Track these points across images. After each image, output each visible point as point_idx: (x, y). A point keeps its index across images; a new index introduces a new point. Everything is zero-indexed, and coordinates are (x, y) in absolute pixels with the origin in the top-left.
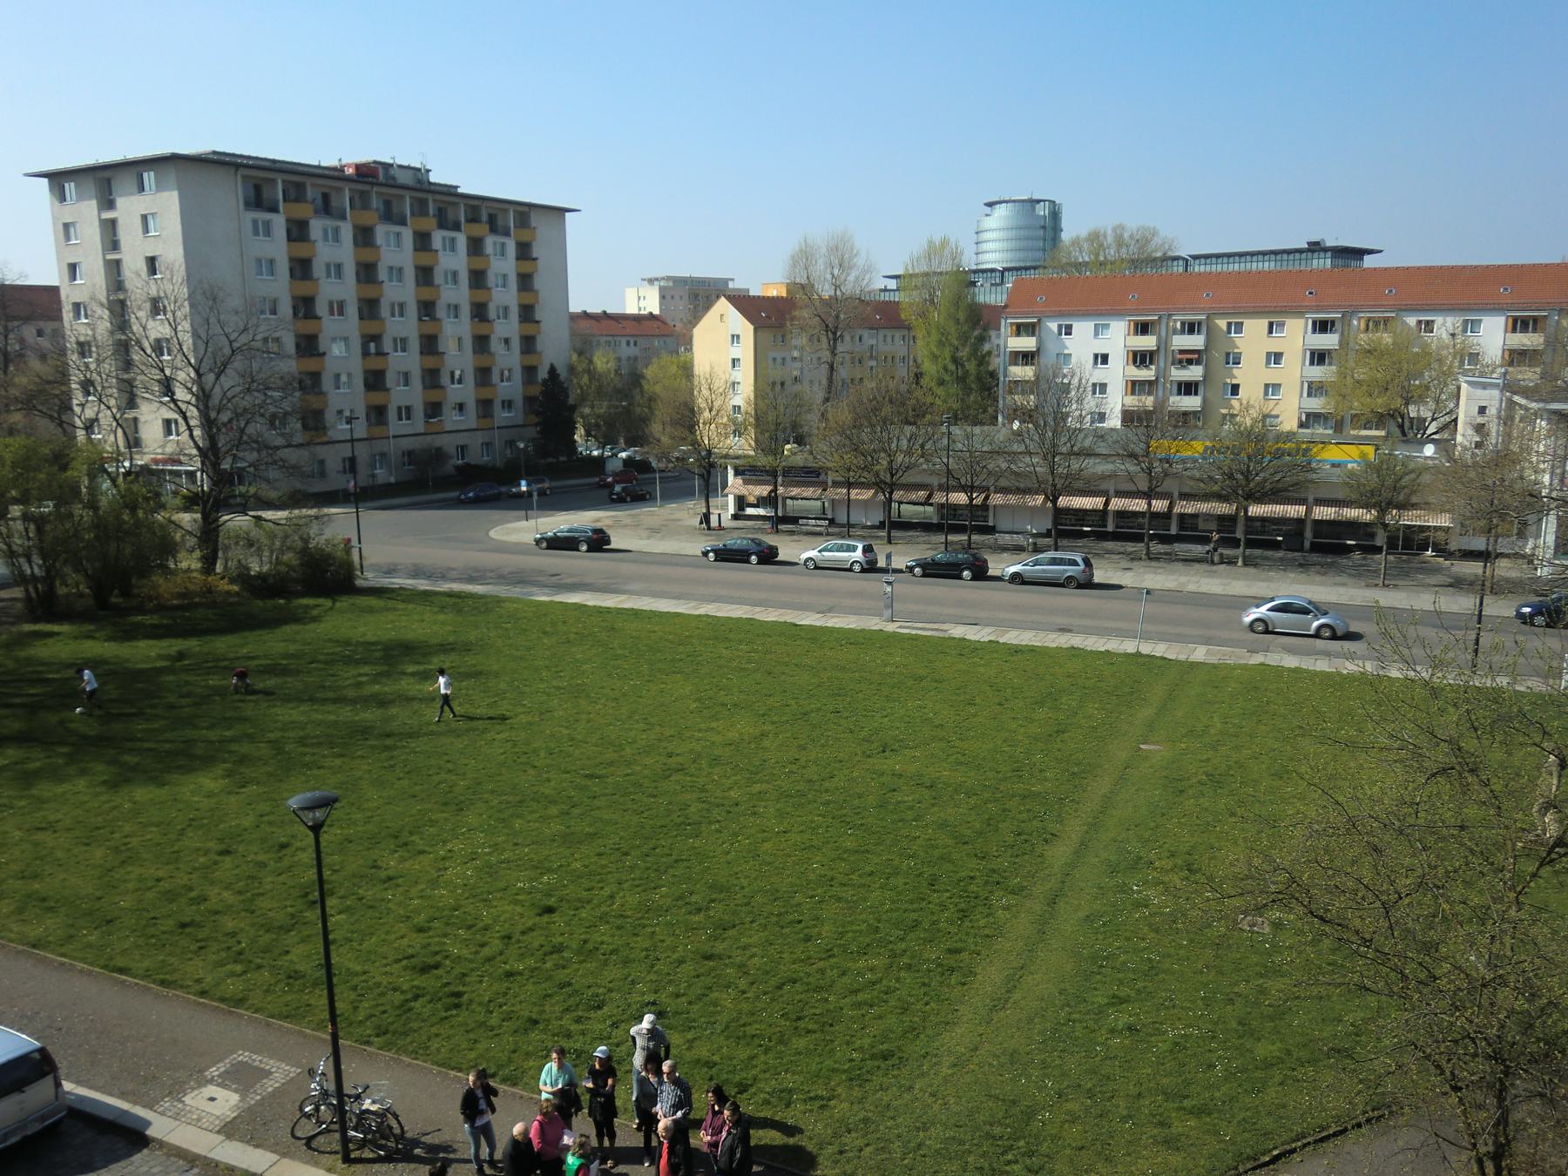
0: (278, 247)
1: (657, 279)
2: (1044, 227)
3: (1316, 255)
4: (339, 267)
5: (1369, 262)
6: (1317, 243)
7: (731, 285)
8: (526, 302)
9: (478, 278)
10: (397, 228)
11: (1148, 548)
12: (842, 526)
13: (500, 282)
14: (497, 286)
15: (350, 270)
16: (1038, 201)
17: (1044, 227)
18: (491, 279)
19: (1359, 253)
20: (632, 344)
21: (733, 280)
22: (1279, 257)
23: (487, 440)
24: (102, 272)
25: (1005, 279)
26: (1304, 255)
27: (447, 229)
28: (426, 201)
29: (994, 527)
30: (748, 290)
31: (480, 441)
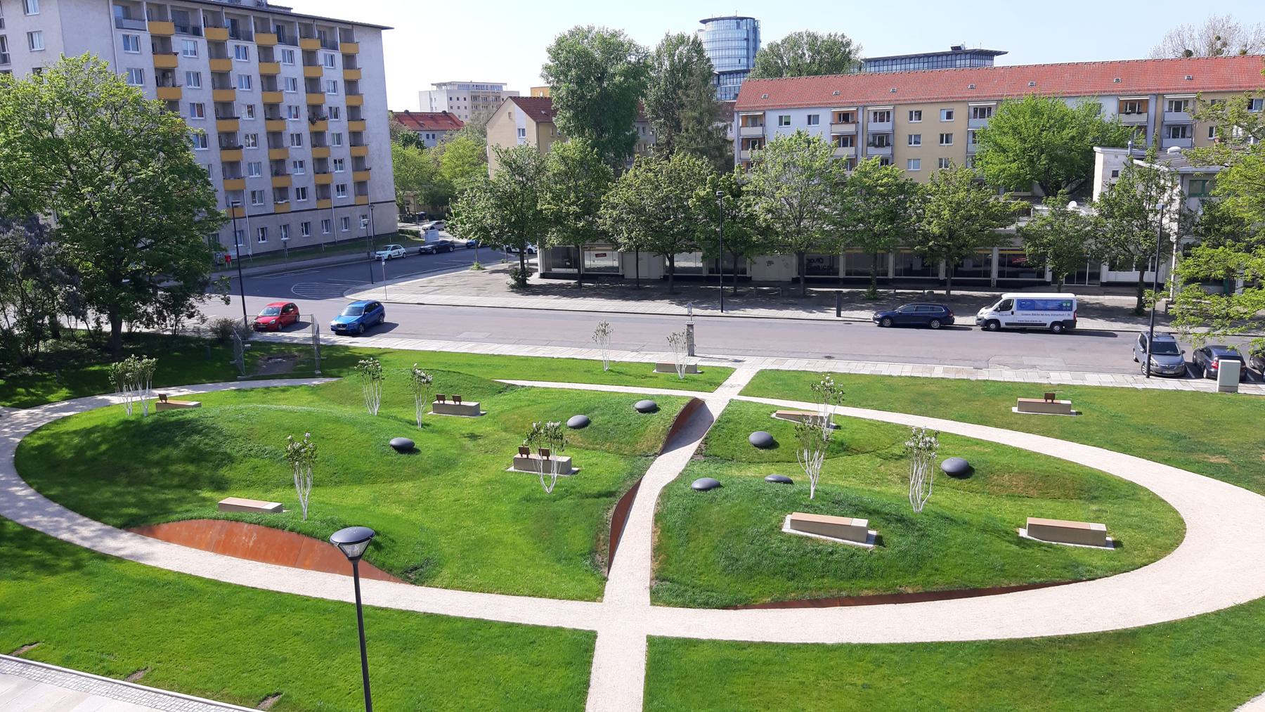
0: (146, 60)
1: (445, 84)
2: (747, 39)
3: (958, 57)
4: (197, 75)
5: (998, 62)
6: (958, 48)
7: (505, 88)
8: (354, 103)
9: (313, 84)
10: (242, 43)
11: (1149, 359)
12: (631, 281)
13: (331, 88)
14: (329, 91)
15: (206, 79)
16: (742, 19)
17: (747, 39)
18: (324, 86)
19: (990, 55)
20: (431, 136)
21: (506, 84)
22: (930, 59)
23: (326, 219)
24: (269, 565)
25: (721, 82)
26: (949, 58)
27: (286, 44)
28: (268, 19)
29: (751, 278)
30: (518, 92)
31: (320, 219)
